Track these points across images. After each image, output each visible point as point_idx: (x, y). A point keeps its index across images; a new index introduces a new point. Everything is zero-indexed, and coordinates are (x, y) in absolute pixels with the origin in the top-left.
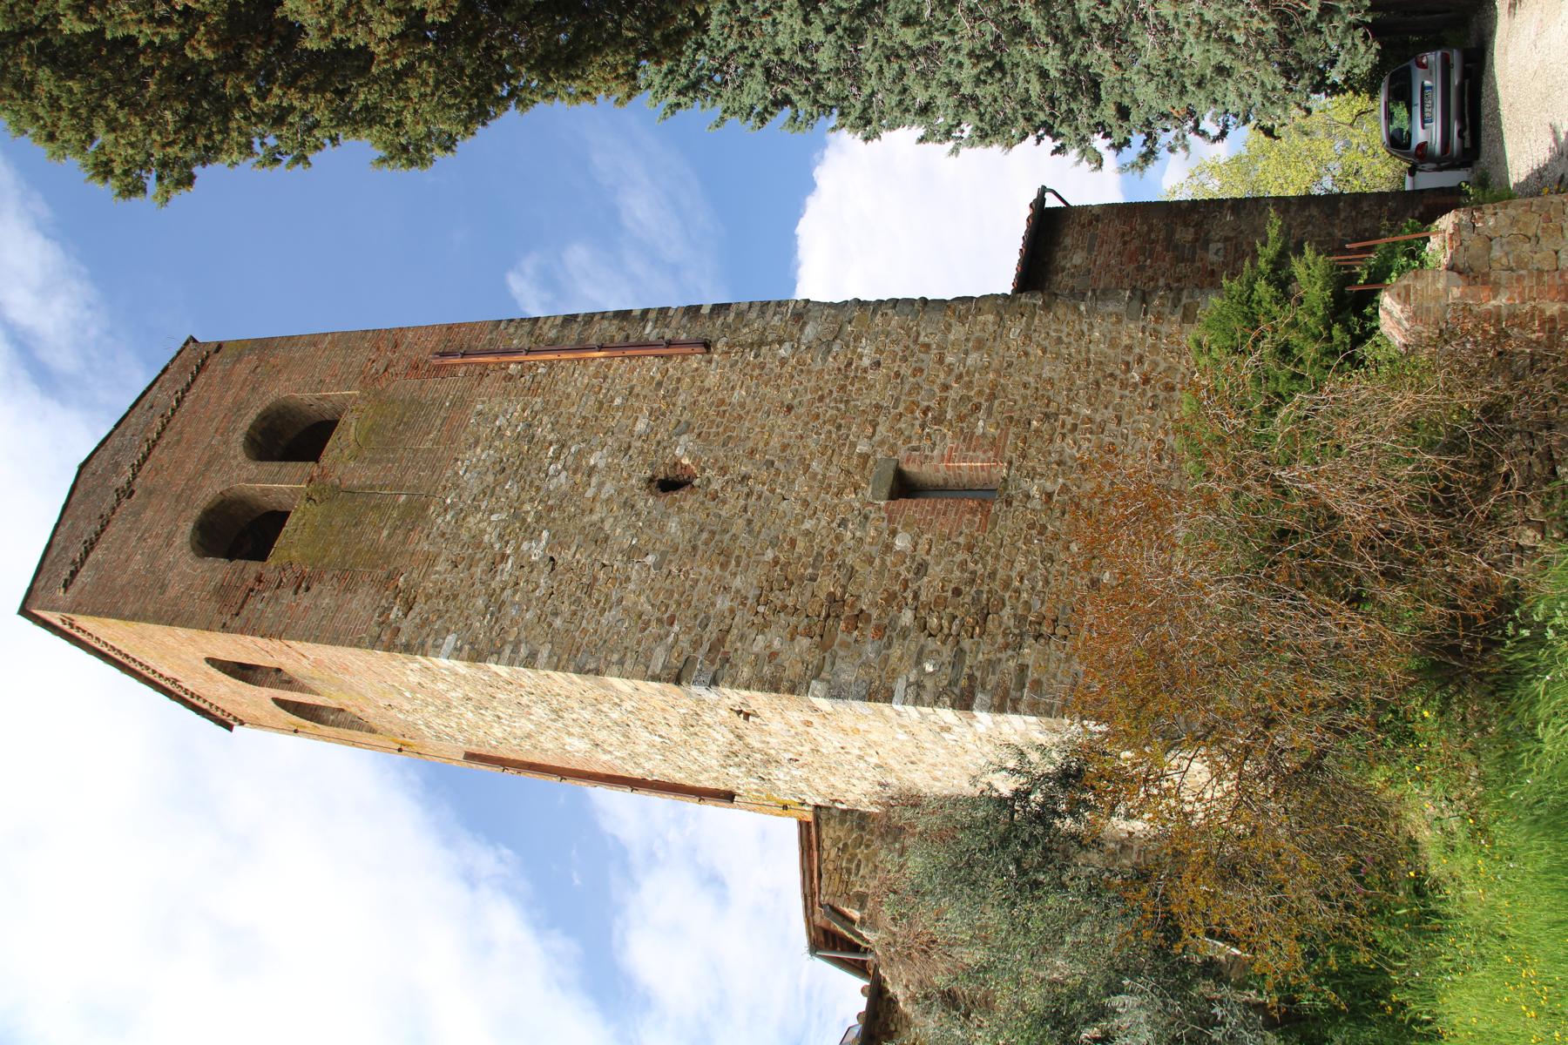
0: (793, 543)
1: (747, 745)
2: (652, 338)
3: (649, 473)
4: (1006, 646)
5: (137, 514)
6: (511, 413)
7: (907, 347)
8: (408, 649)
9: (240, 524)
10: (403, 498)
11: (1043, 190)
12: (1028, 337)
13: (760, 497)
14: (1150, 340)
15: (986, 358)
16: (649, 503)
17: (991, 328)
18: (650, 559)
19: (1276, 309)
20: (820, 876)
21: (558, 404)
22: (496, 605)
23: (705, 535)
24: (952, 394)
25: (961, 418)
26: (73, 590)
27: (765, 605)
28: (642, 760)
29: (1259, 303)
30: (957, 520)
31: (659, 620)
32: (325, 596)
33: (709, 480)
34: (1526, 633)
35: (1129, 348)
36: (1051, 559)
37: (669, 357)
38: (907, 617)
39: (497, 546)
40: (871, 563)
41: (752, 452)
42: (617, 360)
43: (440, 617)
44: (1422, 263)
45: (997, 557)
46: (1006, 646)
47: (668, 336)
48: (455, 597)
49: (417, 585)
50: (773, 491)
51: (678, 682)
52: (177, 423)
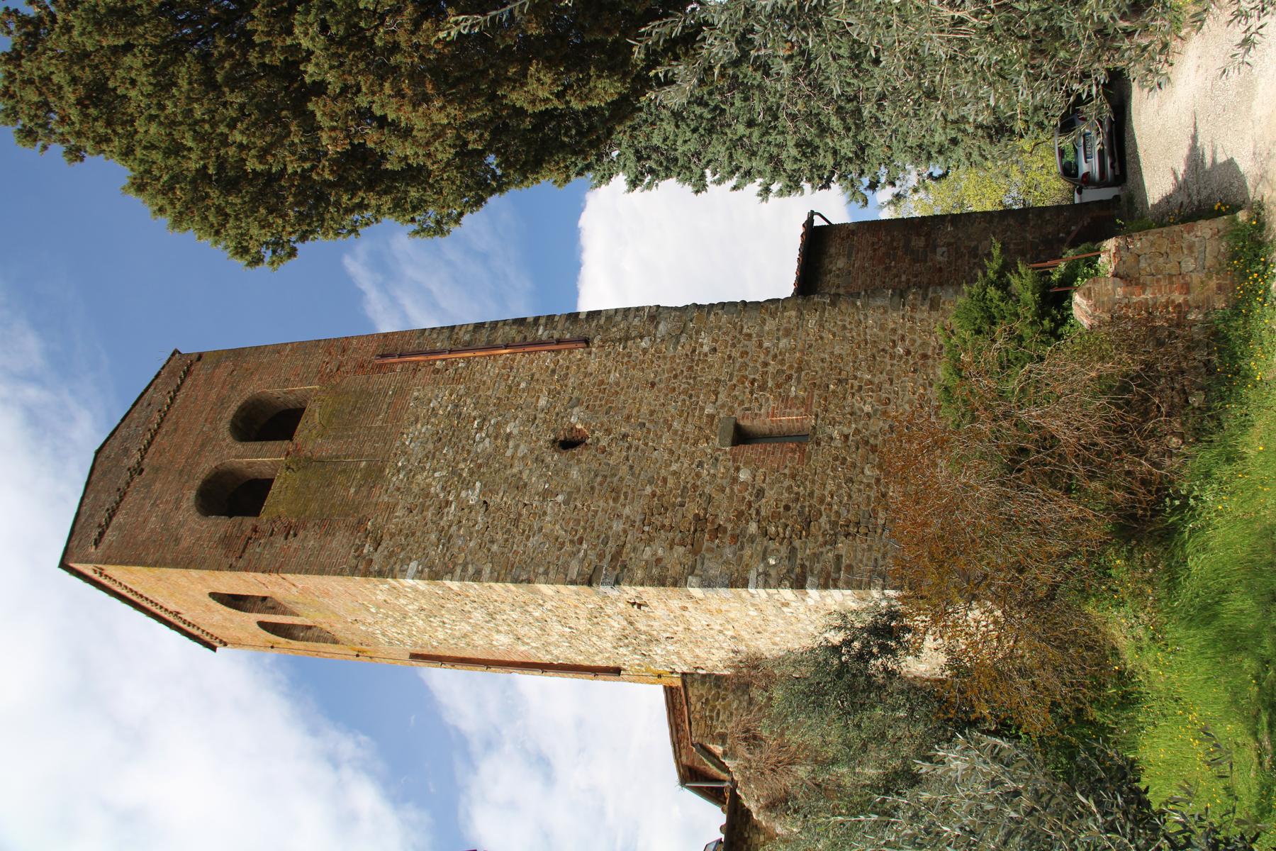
0: (665, 480)
1: (636, 629)
2: (544, 338)
3: (552, 436)
4: (825, 543)
5: (148, 486)
6: (441, 398)
7: (735, 337)
8: (380, 574)
9: (223, 490)
10: (363, 464)
11: (812, 213)
12: (822, 326)
13: (637, 449)
14: (908, 324)
15: (793, 342)
16: (554, 458)
17: (794, 321)
18: (560, 498)
19: (1002, 305)
20: (690, 723)
21: (477, 389)
22: (446, 538)
23: (599, 479)
24: (770, 369)
25: (779, 386)
26: (102, 546)
27: (651, 521)
28: (552, 648)
29: (991, 300)
30: (784, 457)
31: (572, 542)
32: (310, 539)
33: (598, 439)
34: (1177, 503)
35: (894, 331)
36: (851, 480)
37: (559, 352)
38: (753, 528)
39: (442, 495)
40: (723, 491)
41: (629, 417)
42: (519, 355)
43: (403, 549)
44: (1097, 271)
45: (813, 482)
46: (825, 543)
47: (556, 336)
48: (413, 534)
49: (382, 527)
50: (646, 444)
51: (590, 584)
52: (172, 416)
